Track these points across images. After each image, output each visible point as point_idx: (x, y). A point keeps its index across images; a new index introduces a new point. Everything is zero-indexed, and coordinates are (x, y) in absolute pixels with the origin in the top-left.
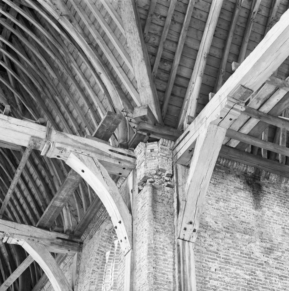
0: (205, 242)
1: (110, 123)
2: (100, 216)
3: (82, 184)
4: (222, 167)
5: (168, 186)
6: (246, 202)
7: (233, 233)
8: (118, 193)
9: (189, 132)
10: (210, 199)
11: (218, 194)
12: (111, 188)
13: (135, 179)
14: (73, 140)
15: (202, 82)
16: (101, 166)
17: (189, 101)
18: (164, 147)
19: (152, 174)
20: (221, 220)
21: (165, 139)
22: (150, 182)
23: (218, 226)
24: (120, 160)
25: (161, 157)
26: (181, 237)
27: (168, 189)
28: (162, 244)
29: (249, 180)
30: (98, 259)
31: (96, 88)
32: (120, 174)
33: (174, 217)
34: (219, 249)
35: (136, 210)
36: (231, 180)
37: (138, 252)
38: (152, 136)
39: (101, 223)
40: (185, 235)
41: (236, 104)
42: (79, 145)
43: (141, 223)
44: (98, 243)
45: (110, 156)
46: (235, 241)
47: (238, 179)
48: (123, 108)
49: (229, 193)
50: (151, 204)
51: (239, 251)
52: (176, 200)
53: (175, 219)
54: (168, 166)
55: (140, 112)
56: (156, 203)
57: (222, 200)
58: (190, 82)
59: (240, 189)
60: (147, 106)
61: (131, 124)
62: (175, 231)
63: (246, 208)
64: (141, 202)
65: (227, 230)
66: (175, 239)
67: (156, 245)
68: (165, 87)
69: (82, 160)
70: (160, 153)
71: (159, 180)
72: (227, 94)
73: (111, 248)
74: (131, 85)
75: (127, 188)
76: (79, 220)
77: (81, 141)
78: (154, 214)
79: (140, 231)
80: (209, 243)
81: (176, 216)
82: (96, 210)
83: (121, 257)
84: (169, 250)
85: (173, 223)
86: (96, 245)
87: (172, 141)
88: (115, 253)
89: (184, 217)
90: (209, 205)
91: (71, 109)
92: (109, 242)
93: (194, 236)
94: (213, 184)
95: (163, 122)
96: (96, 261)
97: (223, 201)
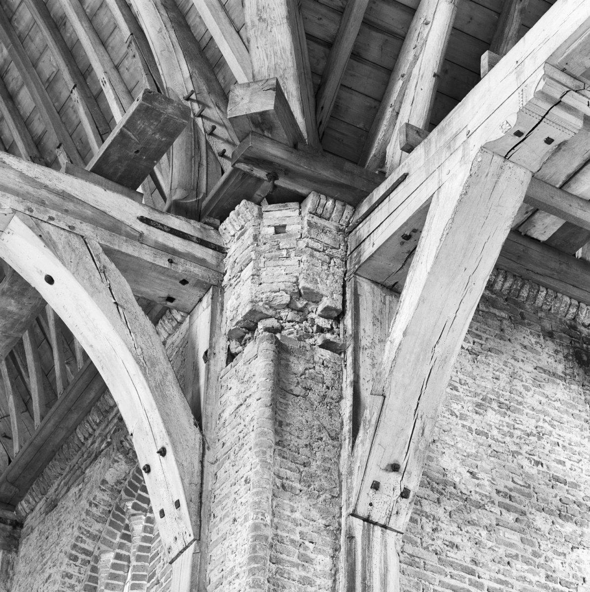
0: (436, 534)
1: (150, 129)
2: (86, 439)
3: (32, 335)
4: (501, 300)
5: (326, 345)
6: (571, 419)
7: (523, 513)
8: (162, 357)
9: (405, 176)
10: (457, 399)
11: (483, 384)
12: (139, 339)
13: (218, 317)
14: (21, 175)
15: (454, 23)
16: (112, 266)
17: (409, 80)
18: (321, 222)
19: (275, 303)
20: (489, 468)
21: (322, 196)
22: (267, 329)
23: (478, 485)
24: (174, 252)
25: (309, 251)
26: (362, 511)
27: (327, 354)
28: (299, 529)
29: (582, 348)
30: (70, 577)
31: (103, 19)
32: (170, 299)
33: (341, 445)
34: (480, 558)
35: (215, 417)
36: (526, 343)
37: (216, 553)
38: (282, 182)
39: (88, 461)
40: (375, 505)
41: (571, 89)
42: (44, 193)
43: (232, 457)
44: (77, 523)
45: (140, 238)
46: (529, 537)
47: (549, 343)
48: (191, 88)
49: (518, 385)
50: (269, 399)
51: (543, 572)
52: (348, 392)
53: (345, 452)
54: (328, 282)
55: (250, 102)
56: (284, 397)
57: (495, 405)
58: (415, 21)
59: (554, 374)
60: (274, 81)
61: (213, 141)
62: (341, 490)
63: (568, 436)
64: (234, 391)
65: (507, 501)
66: (341, 516)
67: (279, 532)
68: (332, 28)
69: (49, 243)
70: (306, 240)
71: (297, 326)
72: (543, 56)
73: (118, 540)
74: (222, 14)
75: (188, 344)
76: (16, 448)
77: (48, 183)
78: (276, 432)
79: (228, 484)
80: (449, 538)
81: (347, 445)
82: (74, 417)
83: (154, 566)
84: (320, 552)
85: (337, 464)
86: (70, 531)
87: (345, 203)
88: (132, 559)
89: (376, 446)
90: (454, 418)
91: (12, 86)
92: (112, 524)
93: (403, 512)
94: (470, 352)
95: (321, 141)
96: (64, 583)
97: (497, 408)
